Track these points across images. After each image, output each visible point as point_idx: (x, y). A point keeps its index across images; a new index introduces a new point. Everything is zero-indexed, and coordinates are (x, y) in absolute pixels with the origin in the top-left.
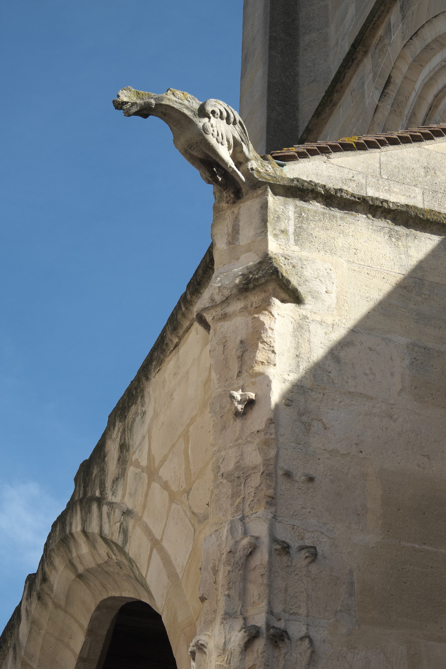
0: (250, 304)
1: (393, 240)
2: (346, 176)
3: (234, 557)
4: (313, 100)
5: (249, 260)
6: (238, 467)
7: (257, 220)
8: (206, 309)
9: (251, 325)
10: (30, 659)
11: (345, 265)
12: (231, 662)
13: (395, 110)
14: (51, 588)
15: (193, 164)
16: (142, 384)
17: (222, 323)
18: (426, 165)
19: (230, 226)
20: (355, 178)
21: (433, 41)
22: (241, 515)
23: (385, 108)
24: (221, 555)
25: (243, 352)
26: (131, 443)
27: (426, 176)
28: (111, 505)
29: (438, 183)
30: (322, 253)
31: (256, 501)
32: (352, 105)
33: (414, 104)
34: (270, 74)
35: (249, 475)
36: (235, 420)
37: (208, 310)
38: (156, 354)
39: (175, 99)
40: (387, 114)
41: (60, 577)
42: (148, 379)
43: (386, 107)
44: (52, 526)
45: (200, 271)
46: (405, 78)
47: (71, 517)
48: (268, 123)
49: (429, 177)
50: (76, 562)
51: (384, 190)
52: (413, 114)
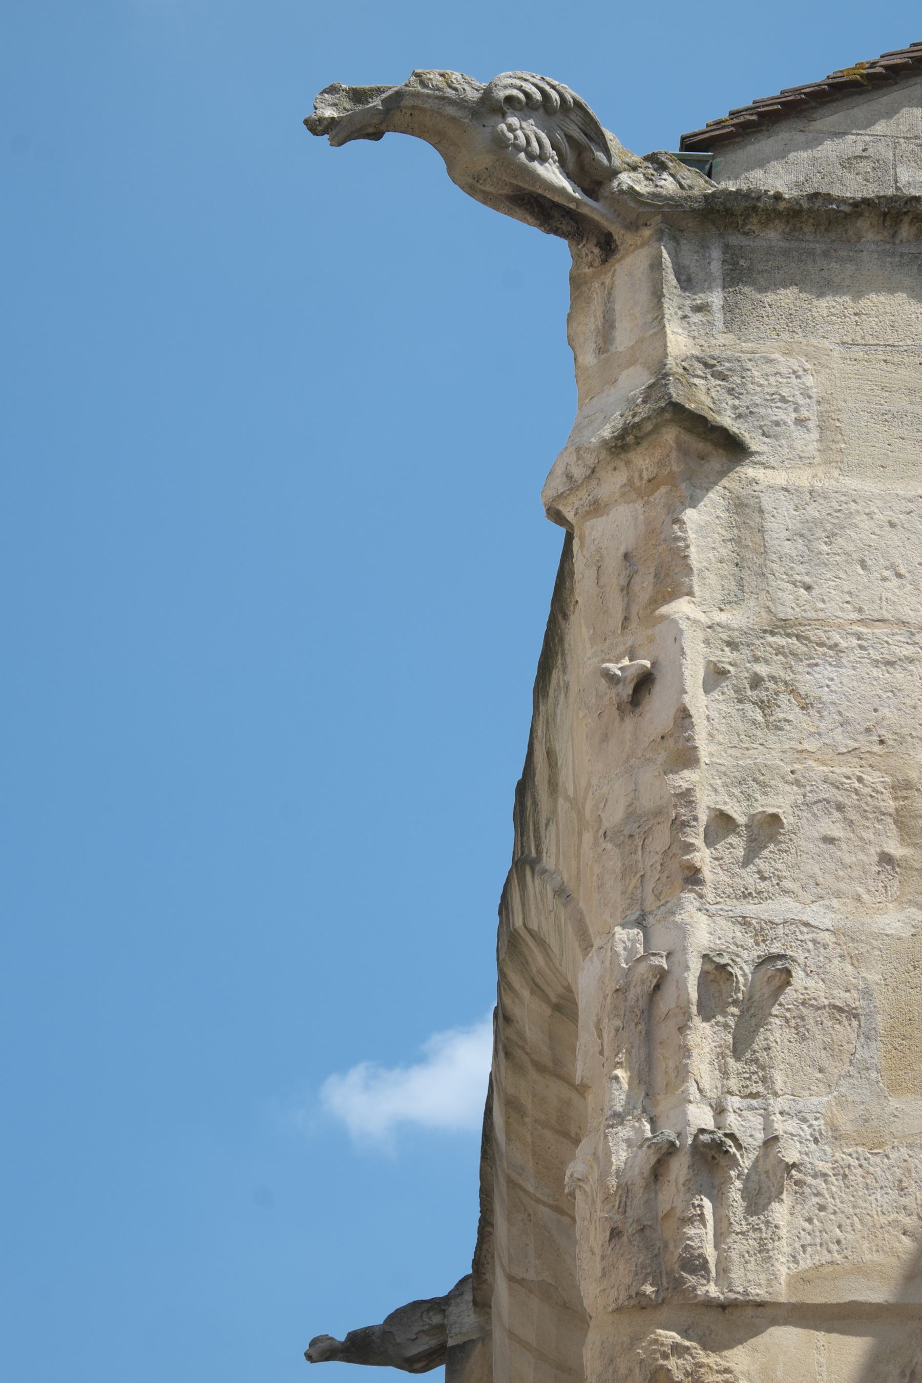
3: (625, 1000)
6: (631, 815)
7: (644, 296)
8: (560, 496)
9: (642, 517)
10: (520, 1175)
11: (837, 352)
12: (628, 1210)
17: (594, 521)
19: (599, 314)
20: (871, 151)
22: (638, 913)
24: (605, 999)
25: (630, 578)
26: (558, 749)
28: (544, 871)
30: (785, 336)
31: (664, 879)
35: (650, 828)
37: (565, 498)
42: (565, 616)
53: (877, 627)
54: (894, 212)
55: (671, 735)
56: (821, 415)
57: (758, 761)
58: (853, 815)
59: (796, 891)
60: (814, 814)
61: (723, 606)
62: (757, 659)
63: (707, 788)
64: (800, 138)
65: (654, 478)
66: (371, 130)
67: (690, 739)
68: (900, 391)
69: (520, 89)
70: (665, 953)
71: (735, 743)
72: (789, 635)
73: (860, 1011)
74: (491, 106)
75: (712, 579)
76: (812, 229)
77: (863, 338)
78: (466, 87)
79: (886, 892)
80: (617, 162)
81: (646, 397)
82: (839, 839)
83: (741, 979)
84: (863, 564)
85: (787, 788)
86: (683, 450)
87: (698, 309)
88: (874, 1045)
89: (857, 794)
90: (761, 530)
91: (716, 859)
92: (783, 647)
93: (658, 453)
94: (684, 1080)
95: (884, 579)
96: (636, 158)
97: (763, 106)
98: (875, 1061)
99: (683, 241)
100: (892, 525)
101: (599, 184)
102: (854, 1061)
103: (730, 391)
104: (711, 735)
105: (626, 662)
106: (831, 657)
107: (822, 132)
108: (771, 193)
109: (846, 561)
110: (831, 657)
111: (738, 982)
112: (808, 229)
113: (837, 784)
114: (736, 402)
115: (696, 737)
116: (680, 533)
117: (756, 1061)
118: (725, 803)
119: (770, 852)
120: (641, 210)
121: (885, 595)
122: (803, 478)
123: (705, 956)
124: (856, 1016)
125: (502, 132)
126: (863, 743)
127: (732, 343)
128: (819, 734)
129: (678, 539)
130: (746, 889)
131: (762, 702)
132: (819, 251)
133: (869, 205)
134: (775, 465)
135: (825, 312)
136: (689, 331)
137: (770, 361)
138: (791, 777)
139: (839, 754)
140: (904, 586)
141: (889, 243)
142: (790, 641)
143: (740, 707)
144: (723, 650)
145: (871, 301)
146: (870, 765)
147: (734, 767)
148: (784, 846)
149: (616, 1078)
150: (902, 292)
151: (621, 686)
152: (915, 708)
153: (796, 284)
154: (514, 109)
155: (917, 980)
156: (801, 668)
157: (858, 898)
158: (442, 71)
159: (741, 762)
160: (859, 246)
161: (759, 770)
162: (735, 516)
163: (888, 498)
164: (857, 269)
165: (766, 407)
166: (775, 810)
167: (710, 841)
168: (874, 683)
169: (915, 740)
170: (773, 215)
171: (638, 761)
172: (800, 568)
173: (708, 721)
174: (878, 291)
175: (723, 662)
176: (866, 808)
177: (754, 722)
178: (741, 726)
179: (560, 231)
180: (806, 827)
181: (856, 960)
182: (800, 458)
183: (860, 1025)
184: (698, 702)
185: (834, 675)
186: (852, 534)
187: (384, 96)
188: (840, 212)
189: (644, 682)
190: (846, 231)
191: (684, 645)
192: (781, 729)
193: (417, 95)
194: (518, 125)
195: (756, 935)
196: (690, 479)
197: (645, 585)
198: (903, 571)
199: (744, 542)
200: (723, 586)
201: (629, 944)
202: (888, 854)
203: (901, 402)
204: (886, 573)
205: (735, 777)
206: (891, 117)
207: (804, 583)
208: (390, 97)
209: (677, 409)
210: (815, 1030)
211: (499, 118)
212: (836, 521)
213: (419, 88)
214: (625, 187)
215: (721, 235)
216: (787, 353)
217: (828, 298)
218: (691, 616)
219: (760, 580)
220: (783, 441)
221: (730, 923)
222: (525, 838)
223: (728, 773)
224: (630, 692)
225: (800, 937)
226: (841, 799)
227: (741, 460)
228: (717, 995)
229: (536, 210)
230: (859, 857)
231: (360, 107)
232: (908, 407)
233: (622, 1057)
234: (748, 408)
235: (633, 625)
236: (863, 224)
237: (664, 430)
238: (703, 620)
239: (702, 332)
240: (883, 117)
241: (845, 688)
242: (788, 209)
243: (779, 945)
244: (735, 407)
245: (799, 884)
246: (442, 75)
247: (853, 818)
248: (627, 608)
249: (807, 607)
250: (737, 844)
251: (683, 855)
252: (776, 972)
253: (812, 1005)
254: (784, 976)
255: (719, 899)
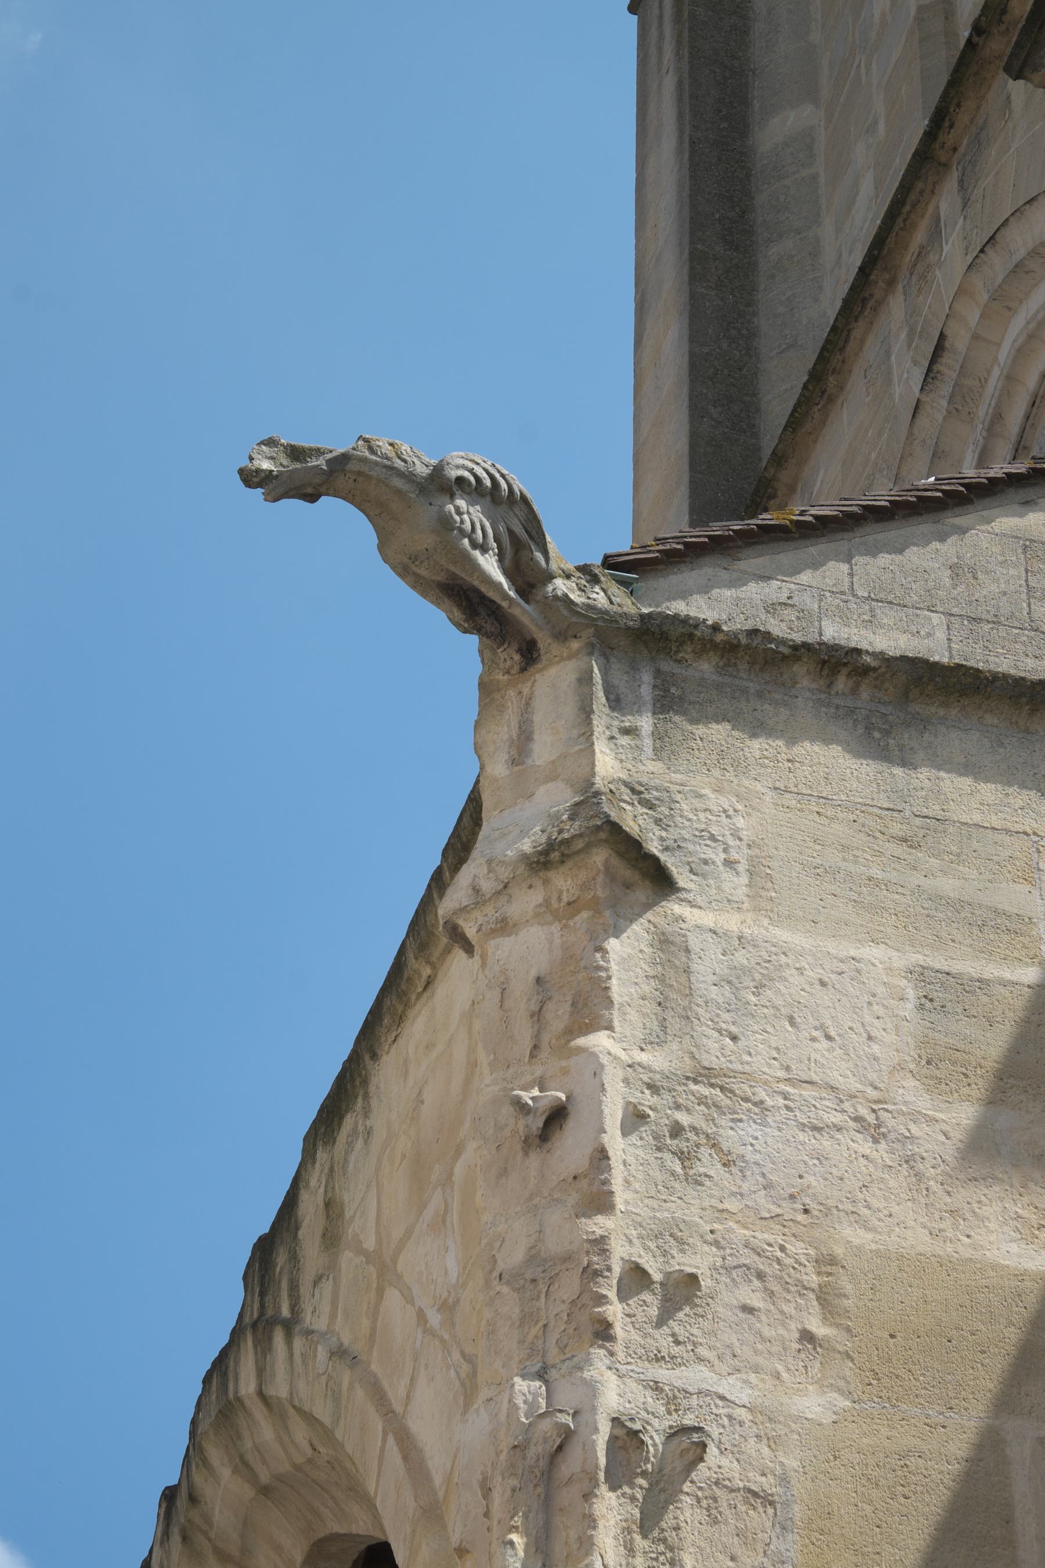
0: (555, 896)
1: (877, 735)
2: (774, 597)
3: (524, 1458)
4: (792, 388)
5: (555, 798)
6: (534, 1257)
7: (570, 709)
8: (463, 910)
9: (558, 941)
11: (769, 797)
13: (957, 410)
14: (207, 1519)
15: (424, 594)
16: (365, 1068)
17: (499, 940)
18: (956, 560)
19: (514, 724)
20: (795, 600)
21: (1028, 254)
22: (540, 1365)
23: (935, 405)
25: (543, 1004)
26: (346, 1198)
27: (955, 586)
28: (309, 1332)
29: (982, 600)
30: (716, 772)
31: (571, 1331)
32: (868, 400)
33: (996, 395)
34: (695, 336)
35: (557, 1274)
36: (526, 1154)
37: (468, 912)
38: (389, 1003)
39: (374, 458)
40: (940, 420)
41: (224, 1492)
42: (374, 1056)
43: (938, 404)
44: (204, 1382)
45: (466, 820)
46: (976, 337)
47: (237, 1362)
48: (693, 446)
49: (961, 588)
50: (252, 1458)
51: (859, 622)
52: (998, 417)
53: (804, 1089)
54: (833, 661)
55: (586, 1176)
56: (751, 859)
57: (676, 1215)
58: (776, 1287)
59: (712, 1360)
60: (733, 1280)
61: (643, 1046)
62: (678, 1107)
63: (623, 1235)
64: (725, 575)
65: (574, 902)
66: (309, 490)
67: (606, 1182)
68: (833, 846)
69: (471, 471)
70: (571, 1411)
71: (653, 1193)
72: (712, 1085)
73: (776, 1498)
74: (440, 484)
75: (633, 1015)
76: (746, 666)
77: (796, 786)
78: (416, 460)
79: (807, 1372)
80: (554, 566)
81: (572, 814)
82: (759, 1310)
83: (651, 1449)
84: (791, 1020)
85: (706, 1248)
86: (611, 875)
87: (626, 731)
88: (790, 1537)
89: (779, 1264)
90: (687, 971)
91: (628, 1315)
92: (706, 1097)
93: (583, 876)
94: (589, 1553)
95: (814, 1039)
96: (570, 566)
97: (691, 537)
98: (791, 1554)
99: (613, 660)
100: (823, 984)
101: (532, 586)
102: (769, 1552)
103: (658, 822)
104: (627, 1181)
105: (536, 1092)
106: (756, 1114)
107: (745, 572)
108: (710, 623)
109: (775, 1015)
110: (756, 1114)
111: (648, 1452)
112: (743, 666)
113: (759, 1250)
114: (664, 834)
115: (613, 1181)
116: (602, 963)
117: (664, 1541)
118: (640, 1256)
119: (686, 1315)
120: (574, 619)
121: (813, 1056)
122: (731, 922)
123: (614, 1420)
124: (772, 1503)
125: (450, 512)
126: (786, 1209)
127: (661, 771)
128: (741, 1195)
129: (599, 968)
130: (659, 1352)
131: (682, 1153)
132: (752, 691)
133: (809, 650)
134: (702, 904)
135: (757, 754)
136: (617, 754)
137: (700, 796)
138: (710, 1237)
139: (761, 1218)
140: (834, 1049)
141: (824, 693)
142: (713, 1092)
143: (659, 1155)
144: (643, 1093)
145: (805, 750)
146: (794, 1235)
147: (650, 1218)
148: (700, 1310)
149: (511, 1543)
150: (838, 744)
151: (531, 1117)
152: (841, 1179)
153: (728, 721)
154: (463, 491)
155: (837, 1472)
156: (724, 1121)
157: (777, 1376)
158: (391, 441)
159: (658, 1215)
160: (793, 692)
161: (677, 1226)
162: (659, 952)
163: (819, 955)
164: (791, 715)
165: (694, 843)
166: (694, 1271)
167: (623, 1296)
168: (800, 1147)
169: (841, 1214)
170: (708, 646)
171: (543, 1201)
172: (726, 1016)
173: (625, 1166)
174: (812, 740)
175: (643, 1105)
176: (788, 1280)
177: (673, 1173)
178: (658, 1175)
179: (483, 630)
180: (724, 1292)
181: (773, 1442)
182: (729, 901)
183: (775, 1514)
184: (616, 1143)
185: (758, 1134)
186: (782, 987)
187: (329, 456)
188: (779, 652)
189: (557, 1116)
190: (781, 674)
191: (605, 1082)
192: (701, 1184)
193: (364, 460)
194: (465, 510)
195: (668, 1403)
196: (614, 906)
197: (560, 1013)
198: (833, 1033)
199: (668, 981)
200: (644, 1024)
201: (530, 1398)
202: (809, 1332)
203: (833, 858)
204: (815, 1034)
205: (651, 1230)
206: (817, 569)
207: (730, 1033)
208: (336, 458)
209: (615, 829)
210: (728, 1513)
211: (447, 498)
212: (765, 972)
213: (367, 454)
214: (559, 593)
215: (653, 659)
216: (718, 790)
217: (761, 740)
218: (613, 1052)
219: (683, 1023)
220: (711, 881)
221: (640, 1387)
222: (269, 1298)
223: (644, 1224)
224: (541, 1125)
225: (715, 1411)
226: (761, 1267)
227: (667, 895)
228: (624, 1463)
229: (464, 604)
230: (779, 1332)
231: (298, 465)
232: (840, 864)
233: (518, 1521)
234: (675, 841)
235: (544, 1055)
236: (799, 669)
237: (595, 850)
238: (623, 1058)
239: (630, 756)
240: (809, 568)
241: (769, 1149)
242: (726, 642)
243: (692, 1416)
244: (662, 839)
245: (715, 1353)
246: (391, 445)
247: (775, 1289)
248: (537, 1036)
249: (732, 1058)
250: (650, 1303)
251: (594, 1307)
252: (690, 1444)
253: (726, 1487)
254: (699, 1451)
255: (629, 1360)
